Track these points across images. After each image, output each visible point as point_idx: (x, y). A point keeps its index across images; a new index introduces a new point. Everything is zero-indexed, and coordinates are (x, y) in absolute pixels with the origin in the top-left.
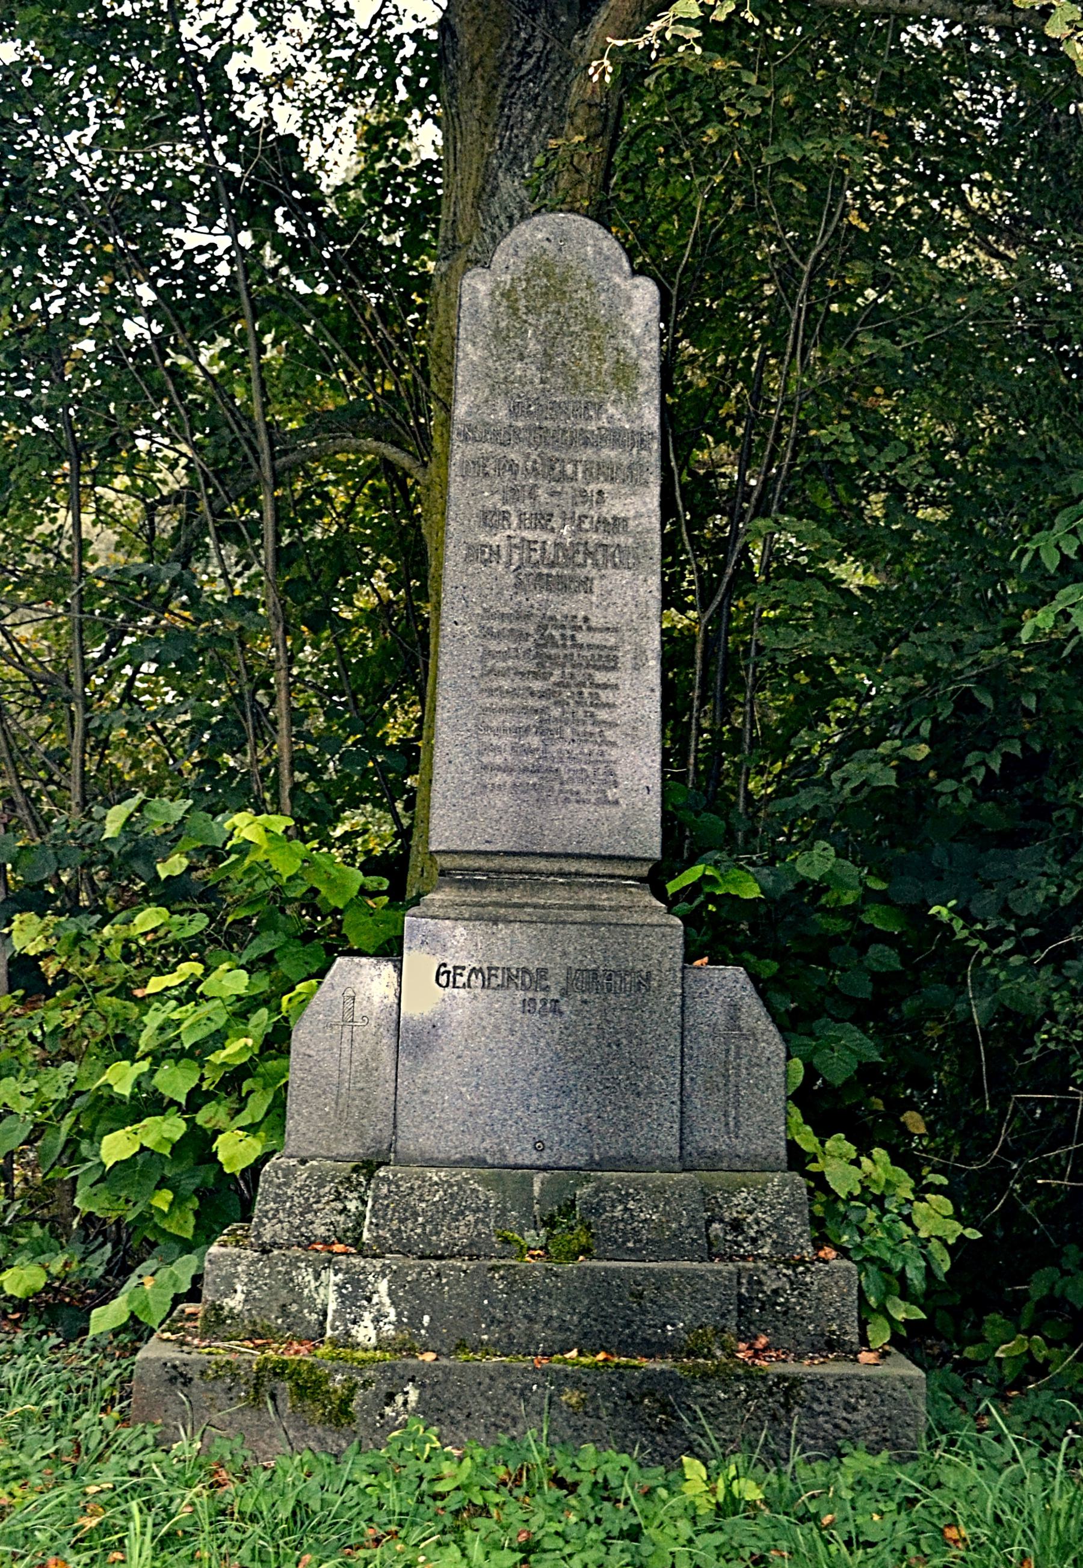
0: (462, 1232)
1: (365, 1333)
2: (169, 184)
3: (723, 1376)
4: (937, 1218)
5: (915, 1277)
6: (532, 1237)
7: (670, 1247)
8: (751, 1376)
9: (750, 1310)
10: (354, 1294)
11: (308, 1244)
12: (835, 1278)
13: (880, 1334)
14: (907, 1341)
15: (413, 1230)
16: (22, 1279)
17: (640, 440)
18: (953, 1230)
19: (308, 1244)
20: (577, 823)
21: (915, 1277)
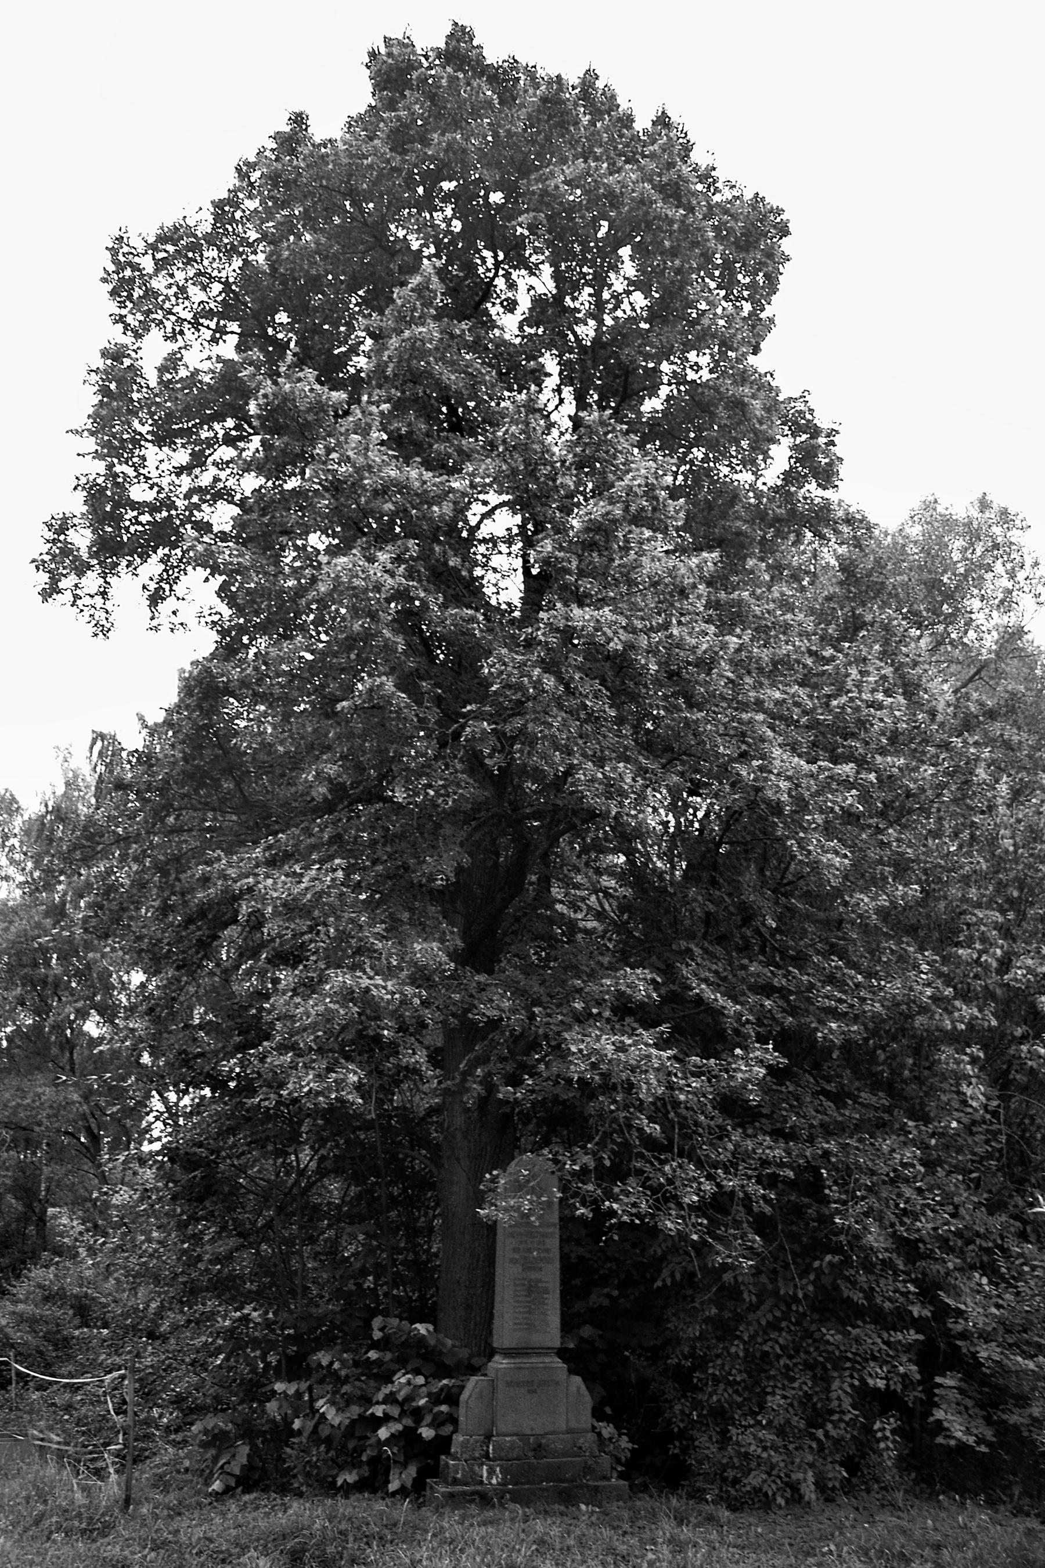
0: (515, 1454)
1: (494, 1481)
2: (608, 1410)
3: (581, 1486)
4: (624, 1442)
5: (623, 1459)
6: (530, 1454)
7: (565, 1454)
8: (588, 1486)
9: (587, 1470)
10: (491, 1472)
11: (475, 1459)
12: (605, 1460)
13: (615, 1475)
14: (621, 1476)
15: (503, 1454)
16: (4, 1261)
17: (554, 1225)
18: (630, 1446)
19: (475, 1459)
20: (538, 1339)
21: (623, 1459)
